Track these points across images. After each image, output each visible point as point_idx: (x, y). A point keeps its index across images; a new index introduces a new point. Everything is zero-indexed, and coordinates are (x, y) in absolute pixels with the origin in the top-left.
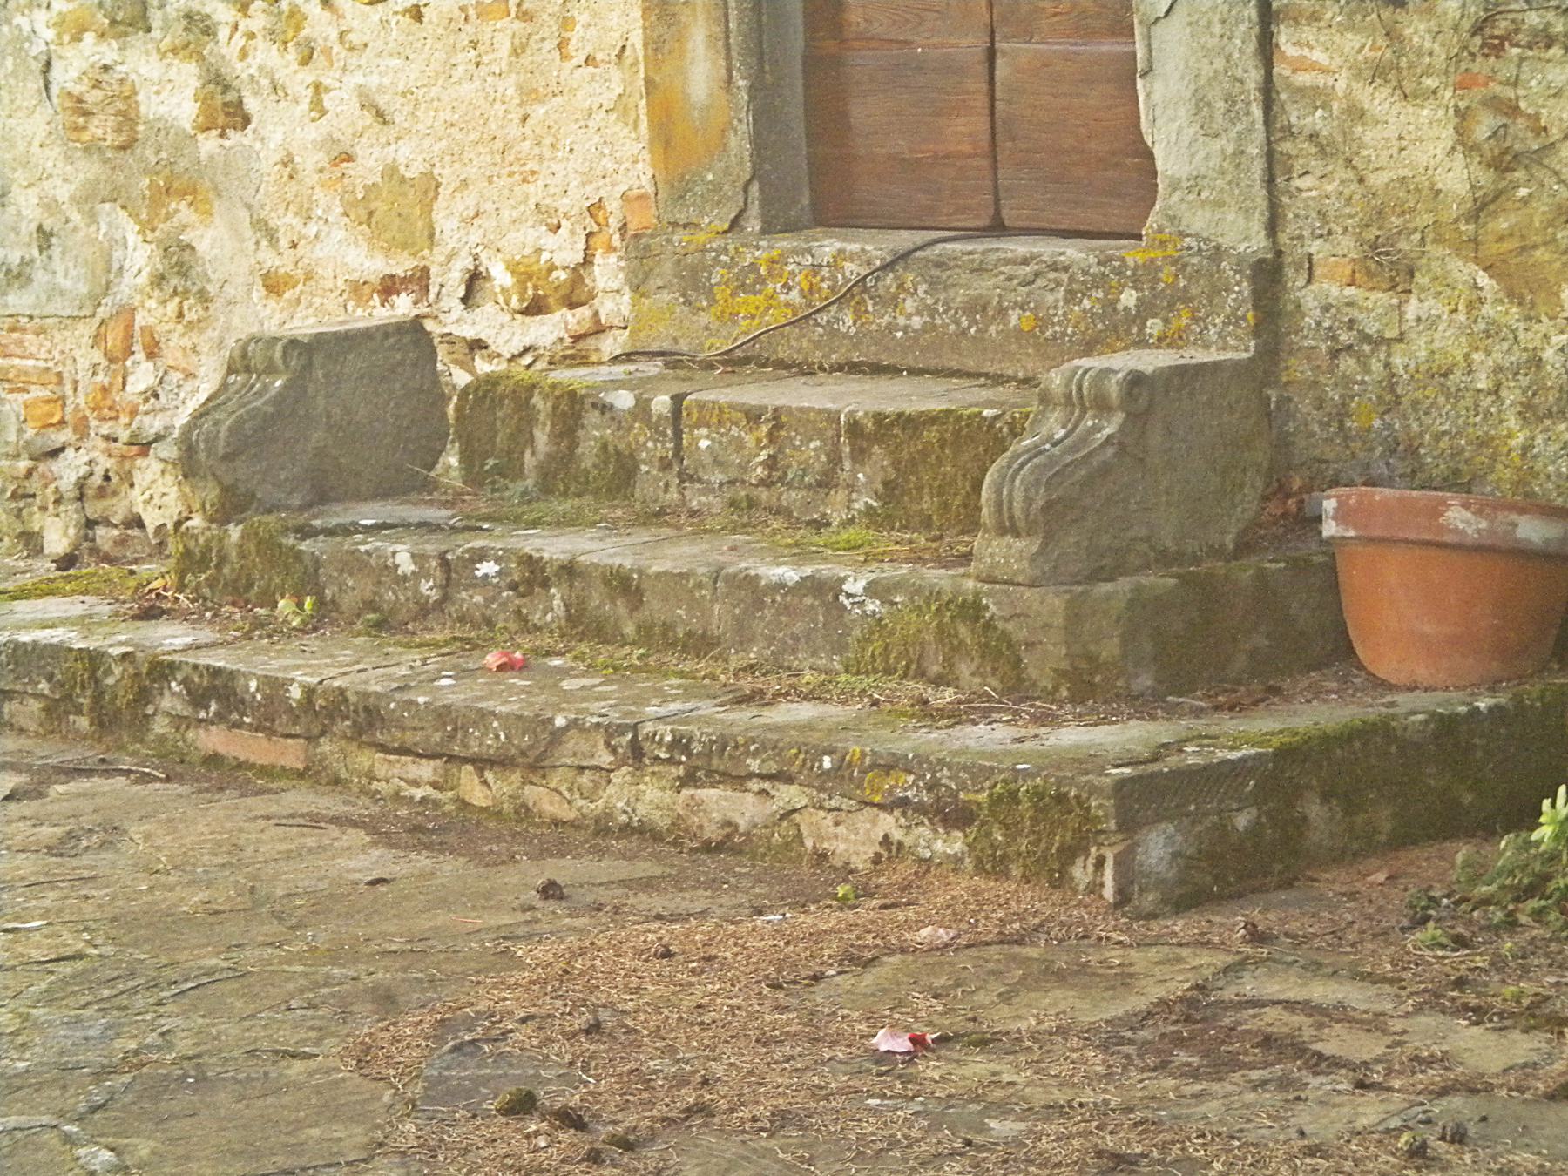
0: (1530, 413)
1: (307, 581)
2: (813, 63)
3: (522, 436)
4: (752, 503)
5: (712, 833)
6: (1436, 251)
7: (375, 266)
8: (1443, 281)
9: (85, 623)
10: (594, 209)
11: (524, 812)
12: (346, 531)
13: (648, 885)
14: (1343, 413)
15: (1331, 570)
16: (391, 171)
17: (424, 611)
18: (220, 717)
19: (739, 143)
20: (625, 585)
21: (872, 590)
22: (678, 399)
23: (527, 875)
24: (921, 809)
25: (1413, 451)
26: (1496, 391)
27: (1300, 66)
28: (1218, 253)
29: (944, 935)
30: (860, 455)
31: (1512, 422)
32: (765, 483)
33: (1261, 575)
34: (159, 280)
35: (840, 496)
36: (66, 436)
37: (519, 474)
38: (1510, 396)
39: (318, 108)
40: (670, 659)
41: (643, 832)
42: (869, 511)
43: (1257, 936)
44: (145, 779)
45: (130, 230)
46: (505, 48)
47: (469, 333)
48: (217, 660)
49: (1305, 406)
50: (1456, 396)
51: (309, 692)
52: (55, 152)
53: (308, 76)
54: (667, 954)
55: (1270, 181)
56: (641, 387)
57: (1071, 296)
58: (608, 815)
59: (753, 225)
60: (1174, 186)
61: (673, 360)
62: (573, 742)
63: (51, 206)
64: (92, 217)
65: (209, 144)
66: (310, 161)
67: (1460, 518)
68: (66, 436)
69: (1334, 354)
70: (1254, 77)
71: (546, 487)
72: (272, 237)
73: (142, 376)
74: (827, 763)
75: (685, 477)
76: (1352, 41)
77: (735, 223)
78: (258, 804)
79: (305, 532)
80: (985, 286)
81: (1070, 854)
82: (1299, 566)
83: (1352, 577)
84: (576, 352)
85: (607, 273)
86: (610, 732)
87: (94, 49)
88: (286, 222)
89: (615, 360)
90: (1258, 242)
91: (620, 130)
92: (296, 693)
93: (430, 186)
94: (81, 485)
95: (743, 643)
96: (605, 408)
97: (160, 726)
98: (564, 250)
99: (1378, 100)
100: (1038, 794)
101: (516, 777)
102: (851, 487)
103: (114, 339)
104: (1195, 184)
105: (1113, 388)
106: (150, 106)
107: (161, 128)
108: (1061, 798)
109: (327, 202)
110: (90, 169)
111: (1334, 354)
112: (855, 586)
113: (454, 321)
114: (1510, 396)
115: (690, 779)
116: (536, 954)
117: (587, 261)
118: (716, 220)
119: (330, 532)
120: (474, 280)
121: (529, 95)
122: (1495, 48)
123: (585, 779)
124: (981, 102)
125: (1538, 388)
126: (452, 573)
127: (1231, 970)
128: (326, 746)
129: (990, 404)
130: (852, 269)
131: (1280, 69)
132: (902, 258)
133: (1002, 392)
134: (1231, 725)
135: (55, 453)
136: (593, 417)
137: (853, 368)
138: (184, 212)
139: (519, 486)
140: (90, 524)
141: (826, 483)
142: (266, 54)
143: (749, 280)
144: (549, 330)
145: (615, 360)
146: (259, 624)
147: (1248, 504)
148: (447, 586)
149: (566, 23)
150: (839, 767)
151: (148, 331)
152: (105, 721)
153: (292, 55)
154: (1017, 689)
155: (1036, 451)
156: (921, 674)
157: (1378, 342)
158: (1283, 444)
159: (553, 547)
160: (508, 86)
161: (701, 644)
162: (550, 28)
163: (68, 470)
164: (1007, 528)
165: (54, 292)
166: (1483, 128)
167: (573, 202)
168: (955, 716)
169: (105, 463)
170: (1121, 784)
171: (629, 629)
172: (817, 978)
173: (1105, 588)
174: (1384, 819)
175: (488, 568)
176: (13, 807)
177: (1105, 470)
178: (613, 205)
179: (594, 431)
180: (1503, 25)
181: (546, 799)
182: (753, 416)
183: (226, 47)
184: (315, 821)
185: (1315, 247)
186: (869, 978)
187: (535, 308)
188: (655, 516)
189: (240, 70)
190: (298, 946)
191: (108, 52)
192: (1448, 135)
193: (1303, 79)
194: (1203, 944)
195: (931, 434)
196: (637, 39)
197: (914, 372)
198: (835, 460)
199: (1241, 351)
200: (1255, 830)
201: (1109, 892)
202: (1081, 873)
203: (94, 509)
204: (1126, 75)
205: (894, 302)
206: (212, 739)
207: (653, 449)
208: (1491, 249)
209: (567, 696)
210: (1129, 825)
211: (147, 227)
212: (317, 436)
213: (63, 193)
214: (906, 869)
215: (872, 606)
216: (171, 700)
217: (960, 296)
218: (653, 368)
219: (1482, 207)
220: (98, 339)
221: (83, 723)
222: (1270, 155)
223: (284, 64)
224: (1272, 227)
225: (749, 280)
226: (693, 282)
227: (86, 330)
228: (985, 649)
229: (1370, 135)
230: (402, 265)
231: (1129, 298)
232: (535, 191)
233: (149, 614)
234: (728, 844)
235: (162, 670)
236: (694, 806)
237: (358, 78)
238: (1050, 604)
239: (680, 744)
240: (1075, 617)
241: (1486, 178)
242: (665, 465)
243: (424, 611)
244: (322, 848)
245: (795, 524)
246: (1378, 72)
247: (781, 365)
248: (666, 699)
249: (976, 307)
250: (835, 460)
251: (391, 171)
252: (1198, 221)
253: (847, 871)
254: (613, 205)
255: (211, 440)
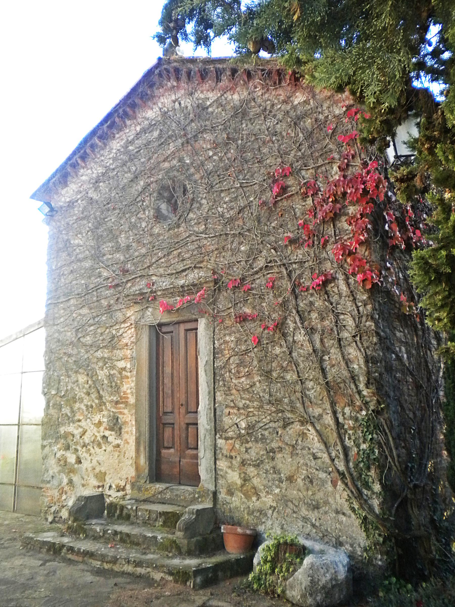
0: (248, 514)
1: (85, 531)
2: (157, 460)
3: (115, 511)
4: (146, 523)
5: (138, 574)
6: (237, 492)
7: (97, 484)
8: (237, 496)
9: (53, 537)
10: (127, 478)
11: (112, 570)
12: (91, 524)
13: (129, 583)
14: (224, 512)
15: (222, 536)
16: (100, 471)
17: (100, 537)
18: (71, 553)
19: (147, 471)
20: (128, 535)
21: (161, 538)
22: (137, 507)
23: (112, 581)
24: (167, 573)
25: (233, 518)
26: (244, 511)
27: (219, 466)
28: (208, 490)
29: (169, 594)
30: (160, 517)
31: (246, 515)
32: (148, 520)
33: (213, 537)
34: (68, 484)
35: (157, 522)
36: (53, 505)
37: (114, 517)
38: (246, 512)
39: (91, 462)
40: (134, 546)
41: (129, 574)
42: (161, 525)
43: (212, 594)
44: (60, 563)
45: (65, 477)
46: (117, 456)
47: (109, 494)
48: (71, 545)
49: (219, 511)
50: (239, 511)
51: (84, 550)
52: (55, 465)
53: (90, 458)
54: (131, 597)
55: (215, 481)
56: (132, 505)
57: (189, 495)
58: (124, 571)
59: (148, 482)
60: (203, 480)
61: (137, 500)
62: (120, 560)
63: (54, 473)
64: (59, 475)
65: (76, 466)
66: (90, 469)
67: (239, 530)
68: (53, 505)
69: (223, 504)
70: (214, 467)
71: (118, 519)
72: (83, 479)
73: (64, 497)
74: (155, 585)
75: (137, 518)
76: (226, 463)
77: (145, 482)
78: (75, 567)
79: (85, 525)
80: (178, 493)
81: (186, 581)
82: (218, 535)
83: (225, 538)
84: (123, 498)
85: (128, 487)
86: (125, 559)
87: (62, 452)
88: (86, 477)
89: (129, 500)
90: (213, 489)
91: (131, 468)
92: (82, 550)
93: (105, 473)
94: (54, 511)
95: (144, 544)
96: (127, 508)
97: (62, 554)
98: (122, 483)
99: (229, 471)
100: (183, 572)
101: (112, 564)
102: (159, 521)
103: (61, 491)
104: (206, 480)
105: (195, 511)
106: (69, 460)
107: (70, 463)
108: (186, 572)
109: (91, 475)
110: (60, 468)
111: (223, 504)
112: (159, 537)
113: (107, 492)
114: (246, 512)
115: (135, 566)
116: (113, 597)
117: (126, 485)
118: (143, 481)
119: (88, 525)
120: (110, 487)
121: (119, 462)
122: (244, 465)
123: (121, 566)
124: (178, 467)
125: (249, 511)
126: (105, 532)
127: (208, 600)
128: (85, 558)
129: (178, 510)
130: (160, 489)
131: (217, 466)
132: (167, 488)
133: (180, 508)
134: (209, 560)
135: (51, 507)
136: (125, 509)
137: (160, 503)
138: (72, 475)
139: (114, 518)
140: (55, 517)
141: (156, 520)
142: (85, 454)
143: (147, 490)
144: (120, 494)
145: (129, 500)
146: (77, 538)
147: (211, 527)
148: (104, 534)
149: (125, 453)
150: (156, 566)
151: (65, 491)
152: (55, 553)
153: (88, 455)
154: (180, 553)
155: (184, 520)
156: (167, 551)
157: (229, 503)
158: (216, 517)
159: (119, 528)
160: (117, 461)
161: (138, 544)
162: (123, 453)
163: (53, 509)
164: (180, 530)
165: (53, 485)
166: (242, 475)
167: (125, 477)
168: (172, 558)
169: (58, 509)
170: (194, 571)
171: (128, 542)
172: (152, 601)
173: (192, 540)
174: (229, 574)
175: (109, 532)
176: (41, 568)
177: (193, 523)
178: (129, 478)
179: (125, 511)
180: (245, 463)
181: (116, 568)
182: (147, 510)
183: (80, 453)
184: (83, 570)
185: (221, 490)
186: (159, 601)
187: (118, 491)
188: (132, 524)
189: (81, 456)
190: (80, 595)
191: (64, 453)
192: (238, 476)
193: (220, 468)
194: (204, 595)
195: (170, 515)
196: (134, 456)
197: (168, 504)
198: (157, 517)
199: (211, 506)
200: (212, 576)
201: (192, 587)
202: (188, 583)
203: (55, 515)
204: (197, 465)
205: (166, 494)
206: (69, 556)
207: (133, 514)
208: (243, 492)
209: (119, 552)
210: (195, 577)
211: (67, 477)
212: (88, 510)
213: (56, 471)
214: (164, 582)
215: (161, 541)
216: (64, 550)
217: (175, 494)
218: (133, 501)
219: (242, 486)
220: (59, 491)
221: (52, 553)
222: (215, 478)
223: (87, 456)
224: (216, 487)
225: (147, 490)
226: (139, 489)
227: (57, 490)
228: (176, 548)
229: (228, 476)
230: (101, 484)
231: (197, 496)
232: (119, 475)
233: (62, 536)
234: (140, 577)
235: (63, 546)
236: (136, 570)
237: (96, 459)
238: (186, 542)
239: (134, 561)
240: (188, 543)
241: (243, 482)
242: (134, 517)
243: (100, 537)
244: (84, 576)
245: (151, 526)
246: (230, 467)
247: (151, 502)
248: (133, 553)
249: (177, 495)
250: (157, 517)
251: (100, 471)
252: (206, 486)
253: (156, 581)
254: (129, 478)
255: (73, 511)
